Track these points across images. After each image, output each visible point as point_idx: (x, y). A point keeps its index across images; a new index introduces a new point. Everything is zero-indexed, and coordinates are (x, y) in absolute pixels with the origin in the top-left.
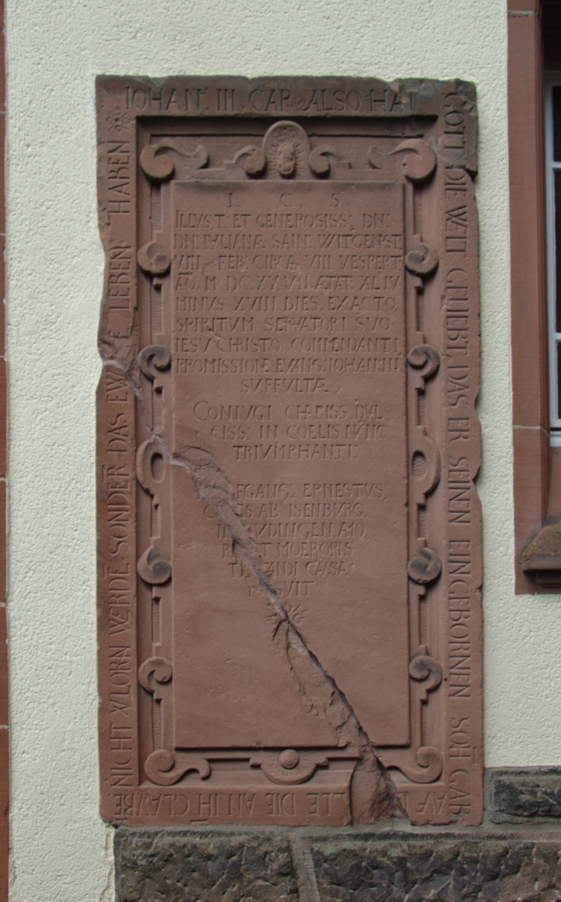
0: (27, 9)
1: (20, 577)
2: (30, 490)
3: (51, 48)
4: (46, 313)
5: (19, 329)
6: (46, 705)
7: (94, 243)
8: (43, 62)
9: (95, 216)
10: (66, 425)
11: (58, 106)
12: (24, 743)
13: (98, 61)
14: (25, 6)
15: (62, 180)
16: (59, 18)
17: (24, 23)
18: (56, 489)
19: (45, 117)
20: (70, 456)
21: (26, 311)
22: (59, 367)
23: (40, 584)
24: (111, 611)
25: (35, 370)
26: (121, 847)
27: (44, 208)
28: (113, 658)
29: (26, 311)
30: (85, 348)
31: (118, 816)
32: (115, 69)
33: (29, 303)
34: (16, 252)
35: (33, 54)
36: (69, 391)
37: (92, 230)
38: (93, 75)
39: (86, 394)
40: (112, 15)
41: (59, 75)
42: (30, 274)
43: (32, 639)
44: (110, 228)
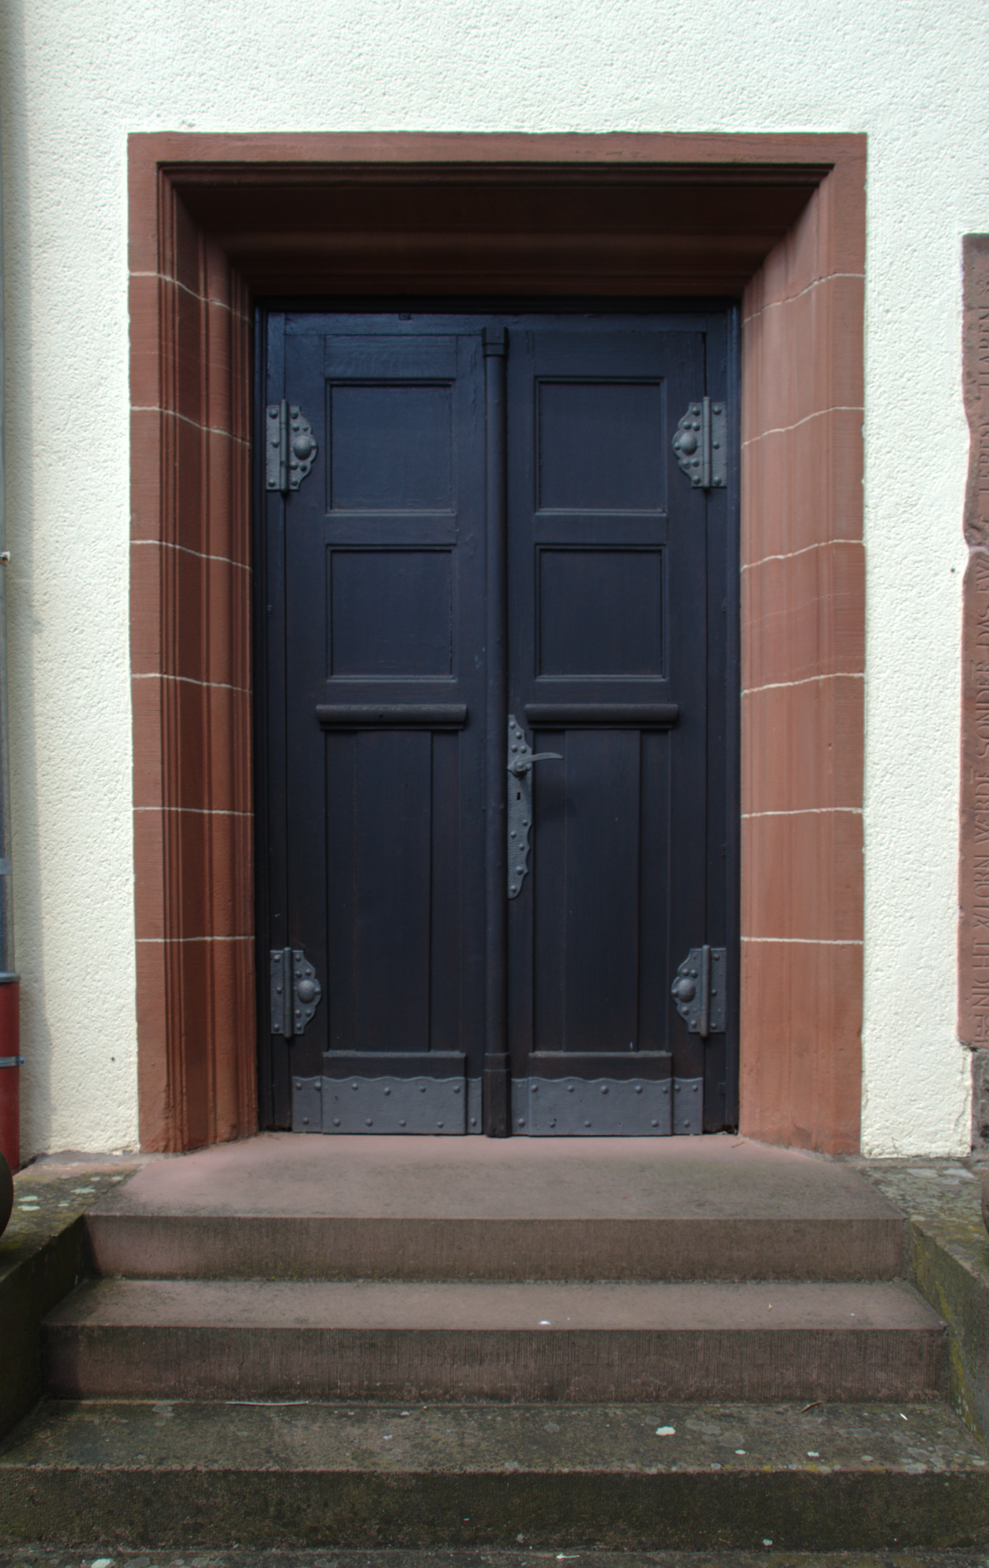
0: (890, 162)
1: (877, 781)
2: (888, 686)
3: (915, 204)
4: (906, 495)
5: (877, 512)
6: (902, 919)
7: (958, 419)
8: (905, 219)
9: (959, 390)
10: (927, 616)
11: (920, 268)
12: (878, 960)
13: (965, 218)
14: (888, 159)
15: (923, 349)
16: (924, 171)
17: (887, 177)
18: (916, 685)
19: (906, 280)
20: (932, 650)
21: (885, 492)
22: (921, 554)
23: (898, 789)
24: (977, 818)
25: (894, 556)
26: (982, 1070)
27: (904, 380)
28: (978, 868)
29: (885, 492)
30: (949, 533)
31: (978, 1038)
32: (982, 226)
33: (887, 484)
34: (874, 427)
35: (894, 211)
36: (932, 579)
37: (956, 404)
38: (959, 233)
39: (951, 584)
40: (981, 166)
41: (923, 234)
42: (889, 452)
43: (888, 848)
44: (980, 403)
